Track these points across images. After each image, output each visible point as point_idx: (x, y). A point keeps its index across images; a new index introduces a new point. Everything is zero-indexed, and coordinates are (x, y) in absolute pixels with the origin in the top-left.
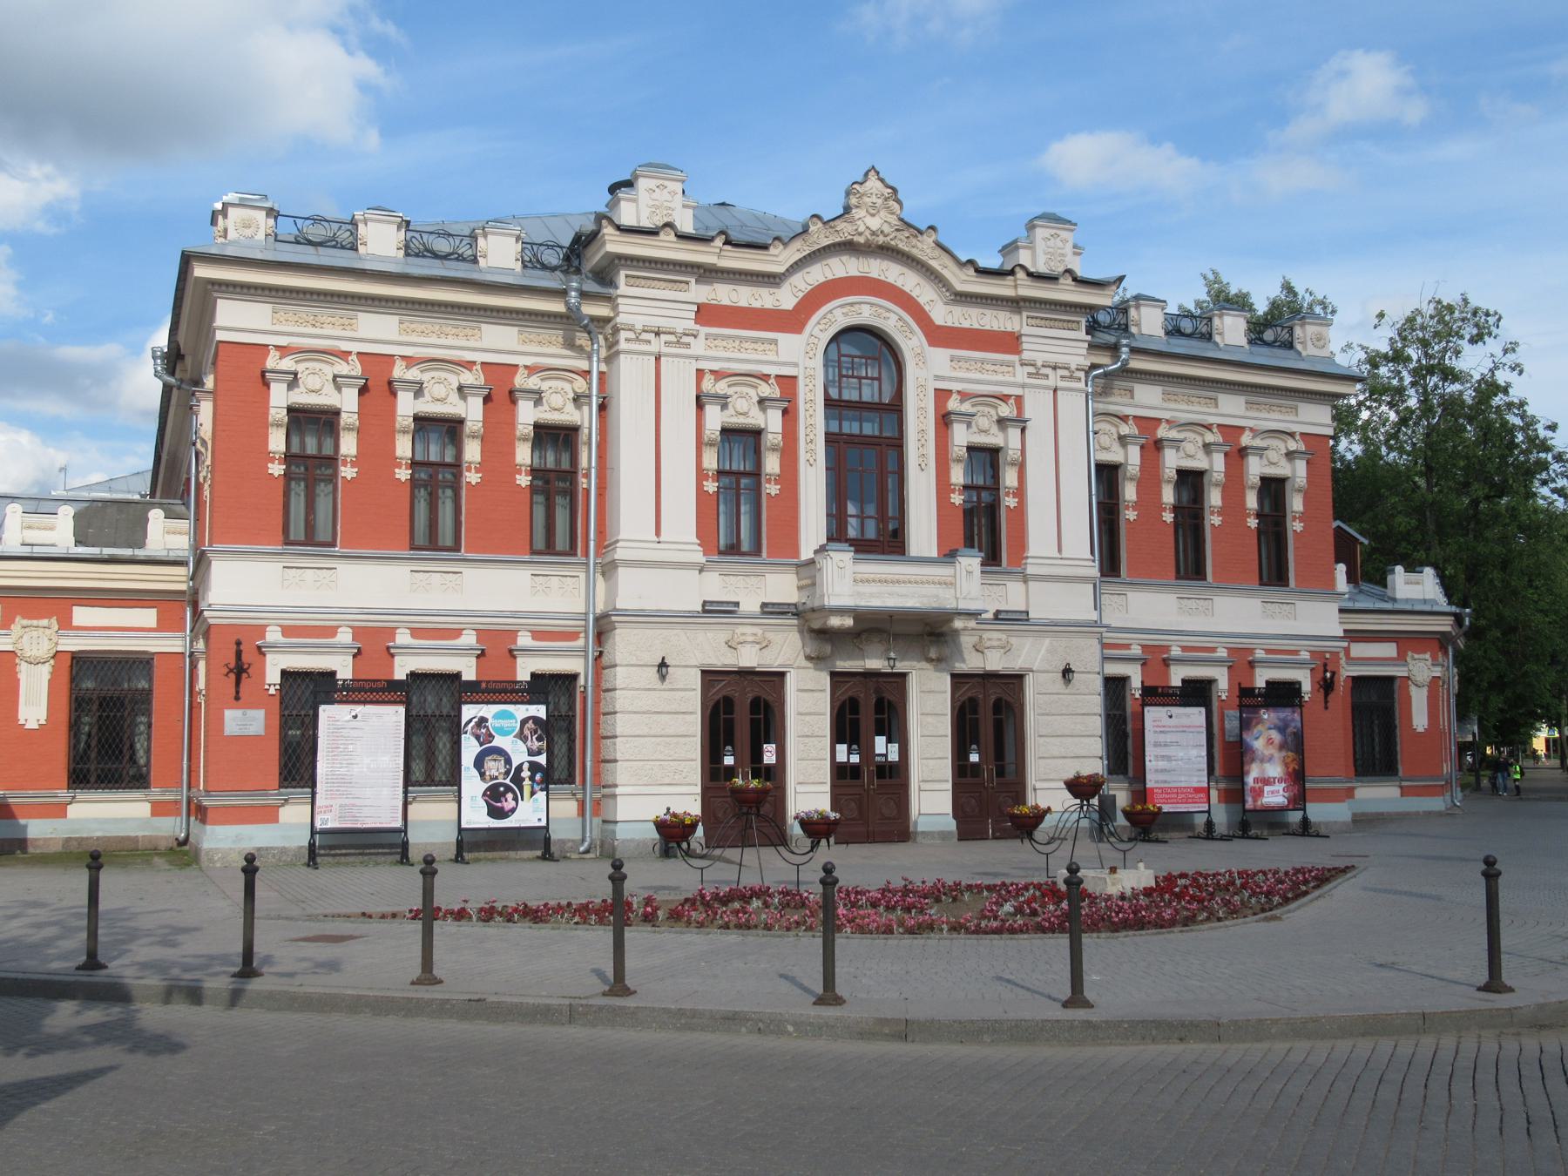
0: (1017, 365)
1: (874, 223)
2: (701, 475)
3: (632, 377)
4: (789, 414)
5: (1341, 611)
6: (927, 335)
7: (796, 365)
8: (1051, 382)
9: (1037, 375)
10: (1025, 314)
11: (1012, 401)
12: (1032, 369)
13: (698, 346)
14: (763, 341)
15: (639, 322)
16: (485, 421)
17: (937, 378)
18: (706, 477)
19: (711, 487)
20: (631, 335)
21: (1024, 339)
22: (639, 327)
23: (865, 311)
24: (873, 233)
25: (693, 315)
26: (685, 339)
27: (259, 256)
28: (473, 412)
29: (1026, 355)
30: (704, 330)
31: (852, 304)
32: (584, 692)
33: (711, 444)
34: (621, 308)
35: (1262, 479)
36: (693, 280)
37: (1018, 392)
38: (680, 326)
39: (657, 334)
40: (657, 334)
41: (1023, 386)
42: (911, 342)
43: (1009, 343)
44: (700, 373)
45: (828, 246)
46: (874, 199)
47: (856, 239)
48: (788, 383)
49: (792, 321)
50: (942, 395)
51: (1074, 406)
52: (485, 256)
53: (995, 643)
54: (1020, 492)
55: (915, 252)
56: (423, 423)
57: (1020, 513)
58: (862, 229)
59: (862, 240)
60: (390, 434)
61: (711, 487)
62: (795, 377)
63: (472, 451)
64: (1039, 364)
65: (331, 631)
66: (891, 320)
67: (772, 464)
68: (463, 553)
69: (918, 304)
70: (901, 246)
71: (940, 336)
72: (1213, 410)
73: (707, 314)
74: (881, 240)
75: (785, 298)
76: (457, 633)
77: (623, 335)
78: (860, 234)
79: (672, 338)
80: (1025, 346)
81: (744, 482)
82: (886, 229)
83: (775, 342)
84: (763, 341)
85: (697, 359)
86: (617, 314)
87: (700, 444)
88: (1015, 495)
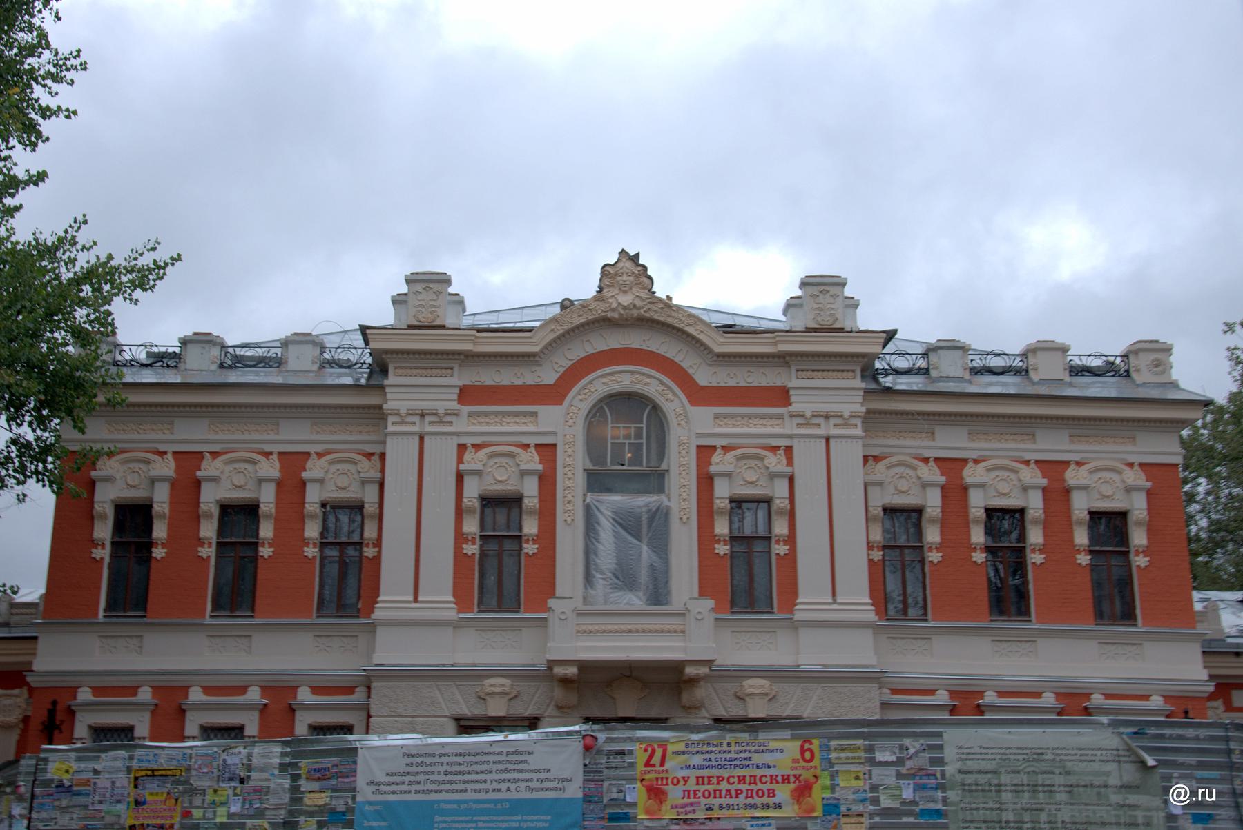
0: (786, 417)
1: (626, 300)
2: (460, 538)
3: (400, 454)
4: (547, 481)
5: (1204, 652)
6: (689, 397)
7: (554, 434)
8: (821, 432)
9: (808, 424)
10: (793, 369)
11: (781, 452)
12: (801, 421)
13: (460, 425)
14: (525, 414)
15: (403, 406)
16: (1045, 510)
17: (699, 436)
18: (466, 541)
19: (471, 549)
20: (396, 419)
21: (792, 392)
22: (441, 411)
23: (624, 379)
24: (625, 308)
25: (455, 397)
26: (448, 419)
27: (1012, 391)
28: (1035, 504)
29: (794, 408)
30: (466, 409)
31: (612, 374)
32: (322, 741)
33: (875, 519)
34: (389, 396)
35: (1091, 513)
36: (456, 369)
37: (787, 443)
38: (441, 407)
39: (422, 415)
40: (422, 415)
41: (791, 437)
42: (673, 403)
43: (781, 396)
44: (462, 448)
45: (583, 325)
46: (625, 278)
47: (609, 315)
48: (547, 451)
49: (554, 394)
50: (705, 452)
51: (848, 455)
52: (1036, 369)
53: (757, 691)
54: (791, 539)
55: (670, 320)
56: (738, 503)
57: (790, 560)
58: (614, 305)
59: (616, 315)
60: (966, 523)
61: (877, 555)
62: (554, 445)
63: (932, 535)
64: (808, 414)
65: (133, 690)
66: (652, 384)
67: (530, 527)
68: (1141, 627)
69: (682, 368)
70: (656, 317)
71: (699, 395)
72: (932, 444)
73: (467, 395)
74: (635, 313)
75: (548, 375)
76: (243, 690)
77: (391, 419)
78: (613, 310)
79: (839, 421)
80: (793, 399)
81: (331, 539)
82: (638, 303)
83: (535, 414)
84: (525, 414)
85: (458, 434)
86: (386, 401)
87: (460, 512)
88: (785, 542)
